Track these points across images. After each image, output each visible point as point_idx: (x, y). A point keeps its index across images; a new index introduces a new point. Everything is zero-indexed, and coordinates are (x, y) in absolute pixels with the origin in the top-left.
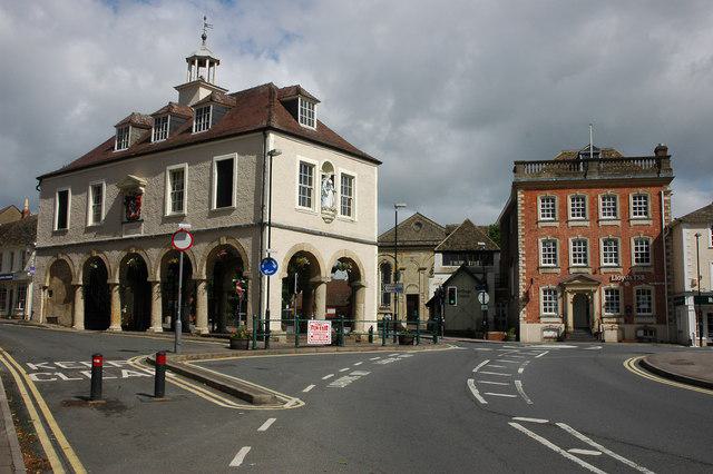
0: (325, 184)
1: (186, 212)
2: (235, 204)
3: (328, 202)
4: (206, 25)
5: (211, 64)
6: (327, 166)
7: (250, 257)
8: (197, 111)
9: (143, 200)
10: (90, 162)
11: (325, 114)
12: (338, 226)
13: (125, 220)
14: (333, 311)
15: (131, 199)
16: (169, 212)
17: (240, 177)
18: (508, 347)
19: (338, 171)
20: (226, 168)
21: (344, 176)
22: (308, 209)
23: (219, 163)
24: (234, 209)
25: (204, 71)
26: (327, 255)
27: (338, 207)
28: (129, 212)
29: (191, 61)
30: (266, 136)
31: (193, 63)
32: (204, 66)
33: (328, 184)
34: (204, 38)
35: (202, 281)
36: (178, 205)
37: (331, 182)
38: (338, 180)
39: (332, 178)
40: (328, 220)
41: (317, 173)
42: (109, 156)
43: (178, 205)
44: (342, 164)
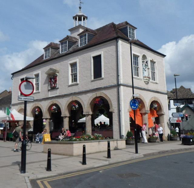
0: (144, 65)
1: (78, 82)
2: (103, 76)
3: (146, 74)
4: (81, 3)
5: (84, 19)
6: (144, 57)
7: (45, 112)
8: (80, 37)
9: (57, 78)
10: (33, 65)
11: (137, 35)
12: (151, 86)
13: (50, 89)
14: (99, 125)
15: (52, 78)
16: (70, 83)
17: (105, 63)
18: (163, 133)
19: (149, 59)
20: (97, 60)
21: (152, 61)
22: (154, 81)
23: (94, 58)
24: (103, 79)
25: (82, 23)
26: (147, 98)
27: (150, 76)
28: (51, 85)
29: (75, 18)
30: (117, 42)
31: (76, 19)
32: (81, 20)
33: (145, 65)
34: (80, 8)
35: (66, 117)
36: (75, 78)
37: (146, 64)
38: (149, 63)
39: (147, 62)
40: (147, 83)
41: (140, 60)
42: (42, 61)
43: (75, 78)
44: (150, 56)
